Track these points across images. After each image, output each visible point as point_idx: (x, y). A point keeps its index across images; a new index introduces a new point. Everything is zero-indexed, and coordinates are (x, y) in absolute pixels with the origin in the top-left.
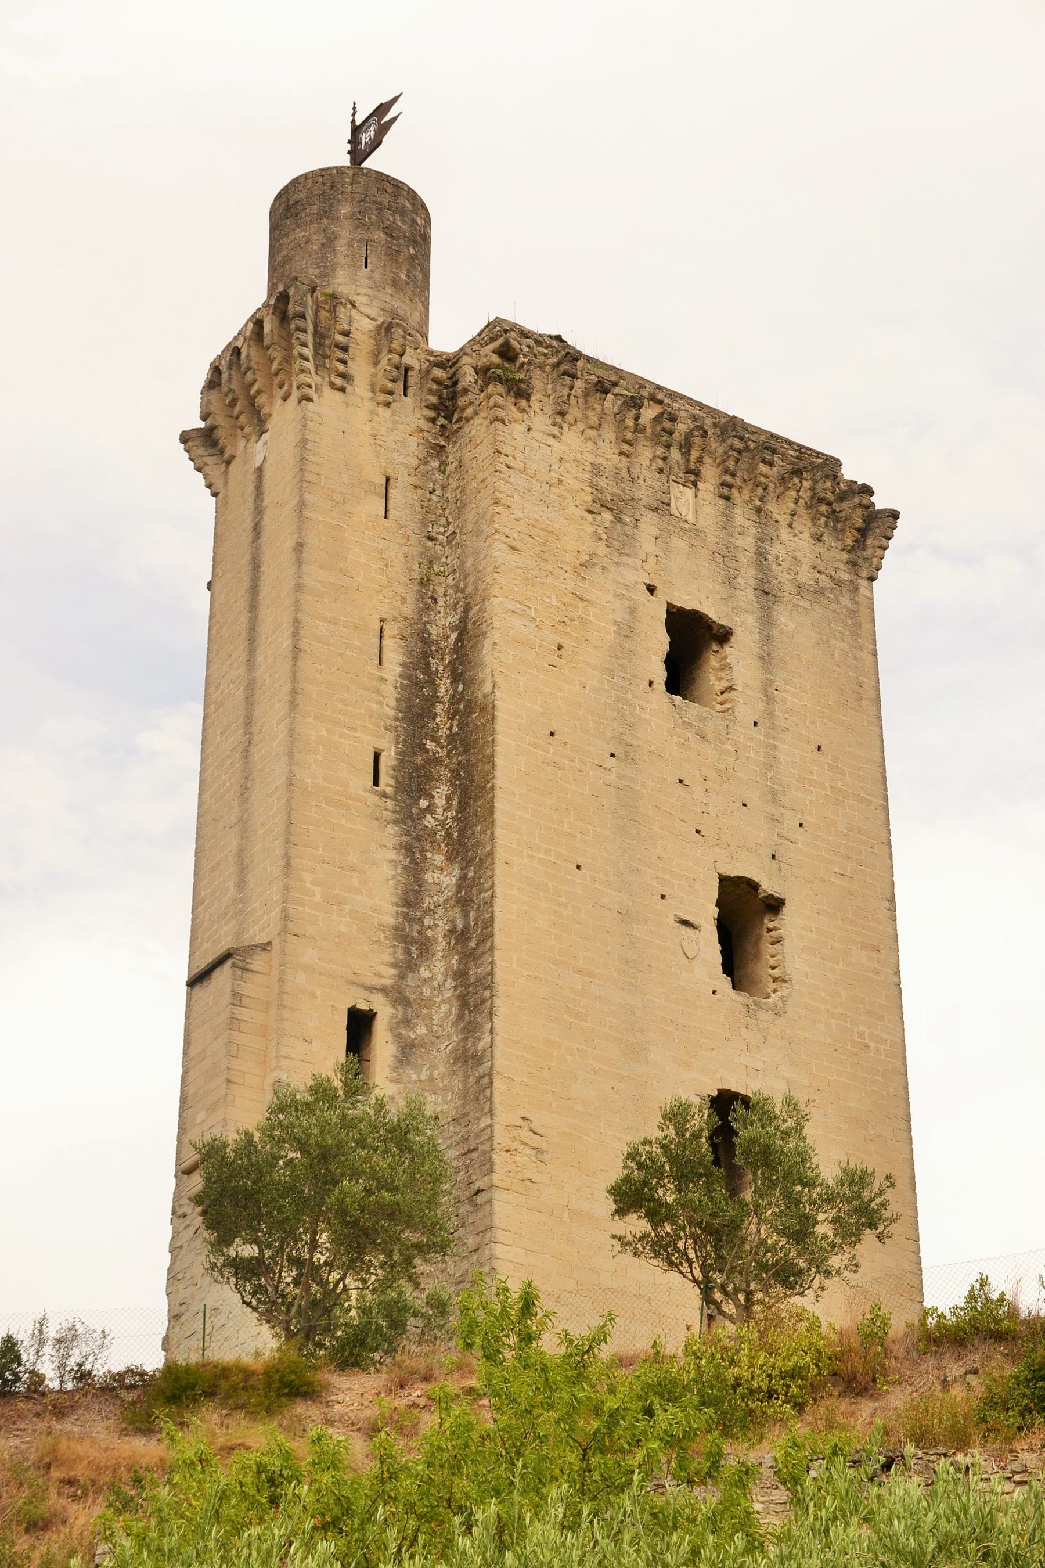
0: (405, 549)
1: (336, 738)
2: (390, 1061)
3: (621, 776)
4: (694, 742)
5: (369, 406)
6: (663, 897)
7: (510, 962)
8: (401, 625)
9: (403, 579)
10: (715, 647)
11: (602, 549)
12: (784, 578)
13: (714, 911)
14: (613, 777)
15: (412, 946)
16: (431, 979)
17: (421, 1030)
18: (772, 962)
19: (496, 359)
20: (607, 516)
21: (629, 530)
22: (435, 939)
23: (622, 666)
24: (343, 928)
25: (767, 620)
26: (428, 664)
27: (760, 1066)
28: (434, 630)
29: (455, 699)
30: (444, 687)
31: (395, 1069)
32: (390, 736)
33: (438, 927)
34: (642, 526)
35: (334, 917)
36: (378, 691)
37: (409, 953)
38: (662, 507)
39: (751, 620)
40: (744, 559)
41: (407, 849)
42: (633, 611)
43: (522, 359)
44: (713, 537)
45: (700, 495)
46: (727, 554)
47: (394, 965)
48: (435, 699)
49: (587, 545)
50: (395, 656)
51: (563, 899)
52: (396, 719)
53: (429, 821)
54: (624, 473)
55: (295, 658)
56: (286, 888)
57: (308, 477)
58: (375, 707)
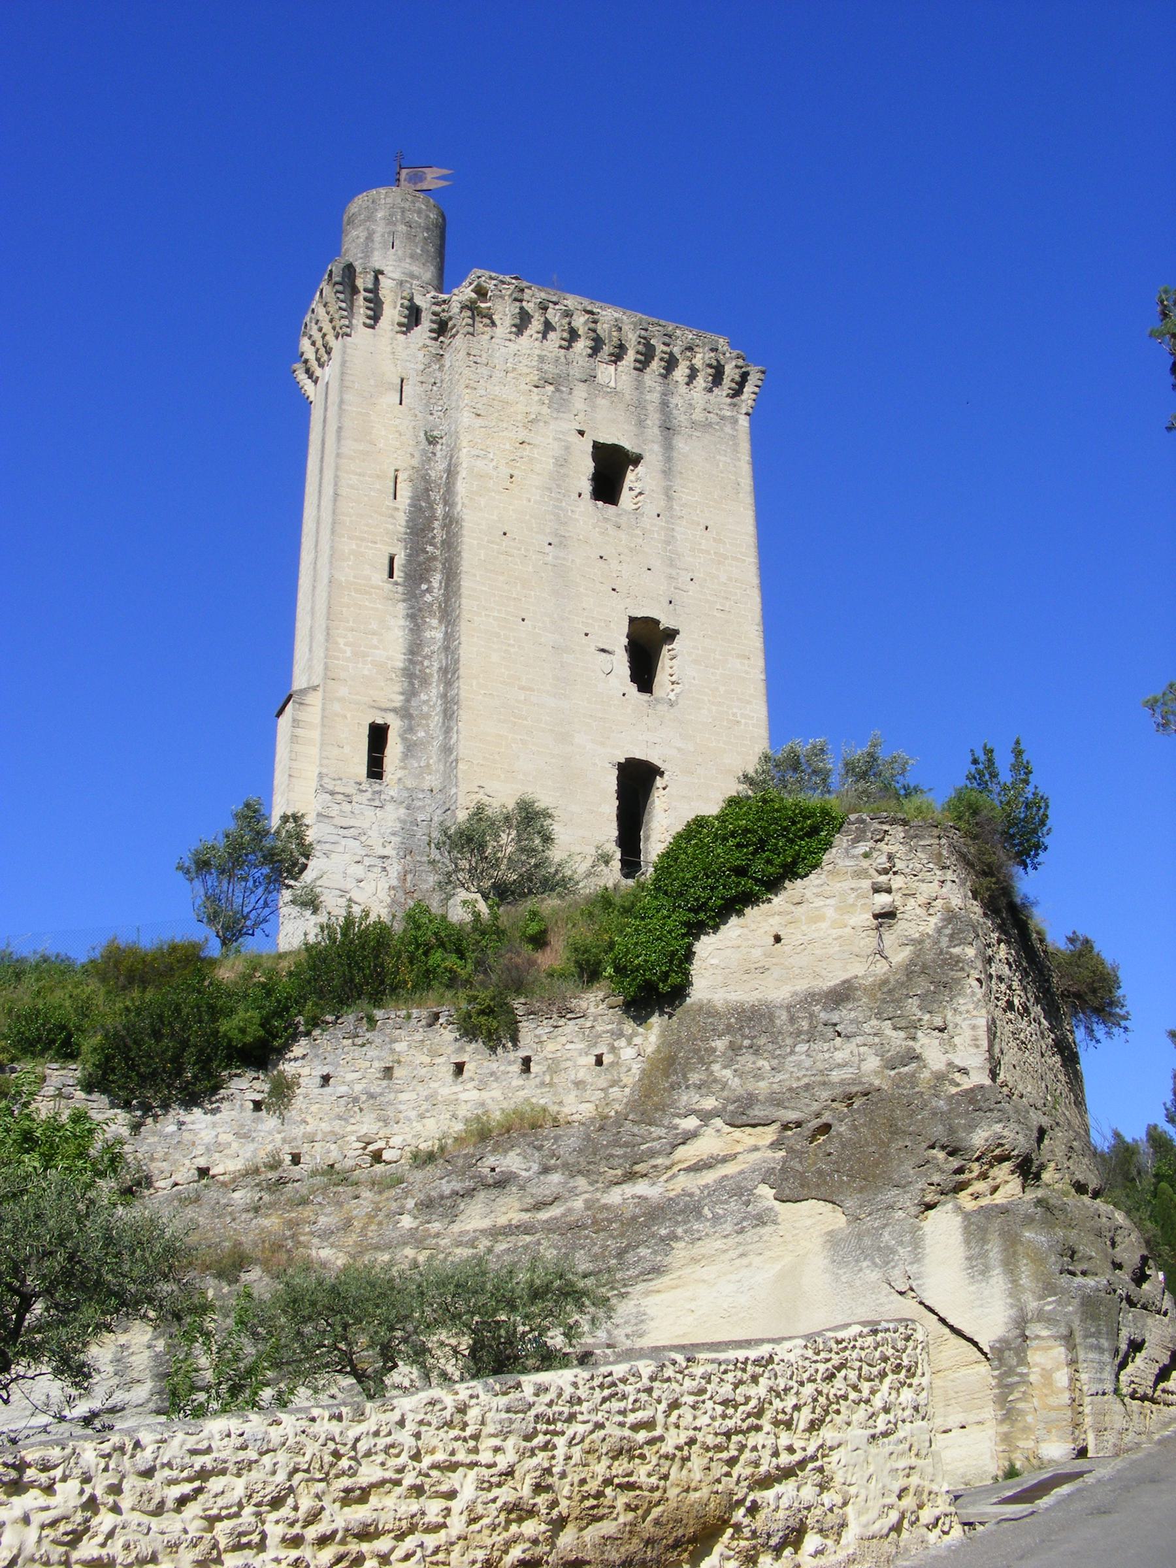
0: (413, 423)
1: (362, 550)
2: (399, 755)
3: (556, 558)
4: (612, 531)
5: (390, 334)
6: (586, 635)
7: (468, 688)
8: (411, 472)
9: (411, 443)
10: (631, 467)
11: (545, 410)
12: (682, 418)
13: (625, 641)
14: (550, 559)
15: (413, 677)
16: (428, 701)
17: (421, 734)
18: (670, 671)
19: (474, 295)
20: (551, 388)
21: (565, 396)
22: (432, 675)
23: (558, 486)
24: (366, 672)
25: (668, 447)
26: (429, 496)
27: (659, 740)
28: (433, 474)
29: (447, 515)
30: (440, 511)
31: (402, 760)
32: (401, 545)
33: (433, 667)
34: (575, 392)
35: (360, 665)
36: (392, 516)
37: (412, 684)
38: (590, 378)
39: (656, 447)
40: (650, 408)
41: (412, 617)
42: (567, 448)
43: (490, 294)
44: (628, 392)
45: (620, 369)
46: (638, 408)
47: (402, 694)
48: (433, 517)
49: (535, 409)
50: (405, 492)
51: (512, 642)
52: (406, 533)
53: (428, 598)
54: (563, 360)
55: (335, 500)
56: (327, 649)
57: (347, 384)
58: (391, 527)
